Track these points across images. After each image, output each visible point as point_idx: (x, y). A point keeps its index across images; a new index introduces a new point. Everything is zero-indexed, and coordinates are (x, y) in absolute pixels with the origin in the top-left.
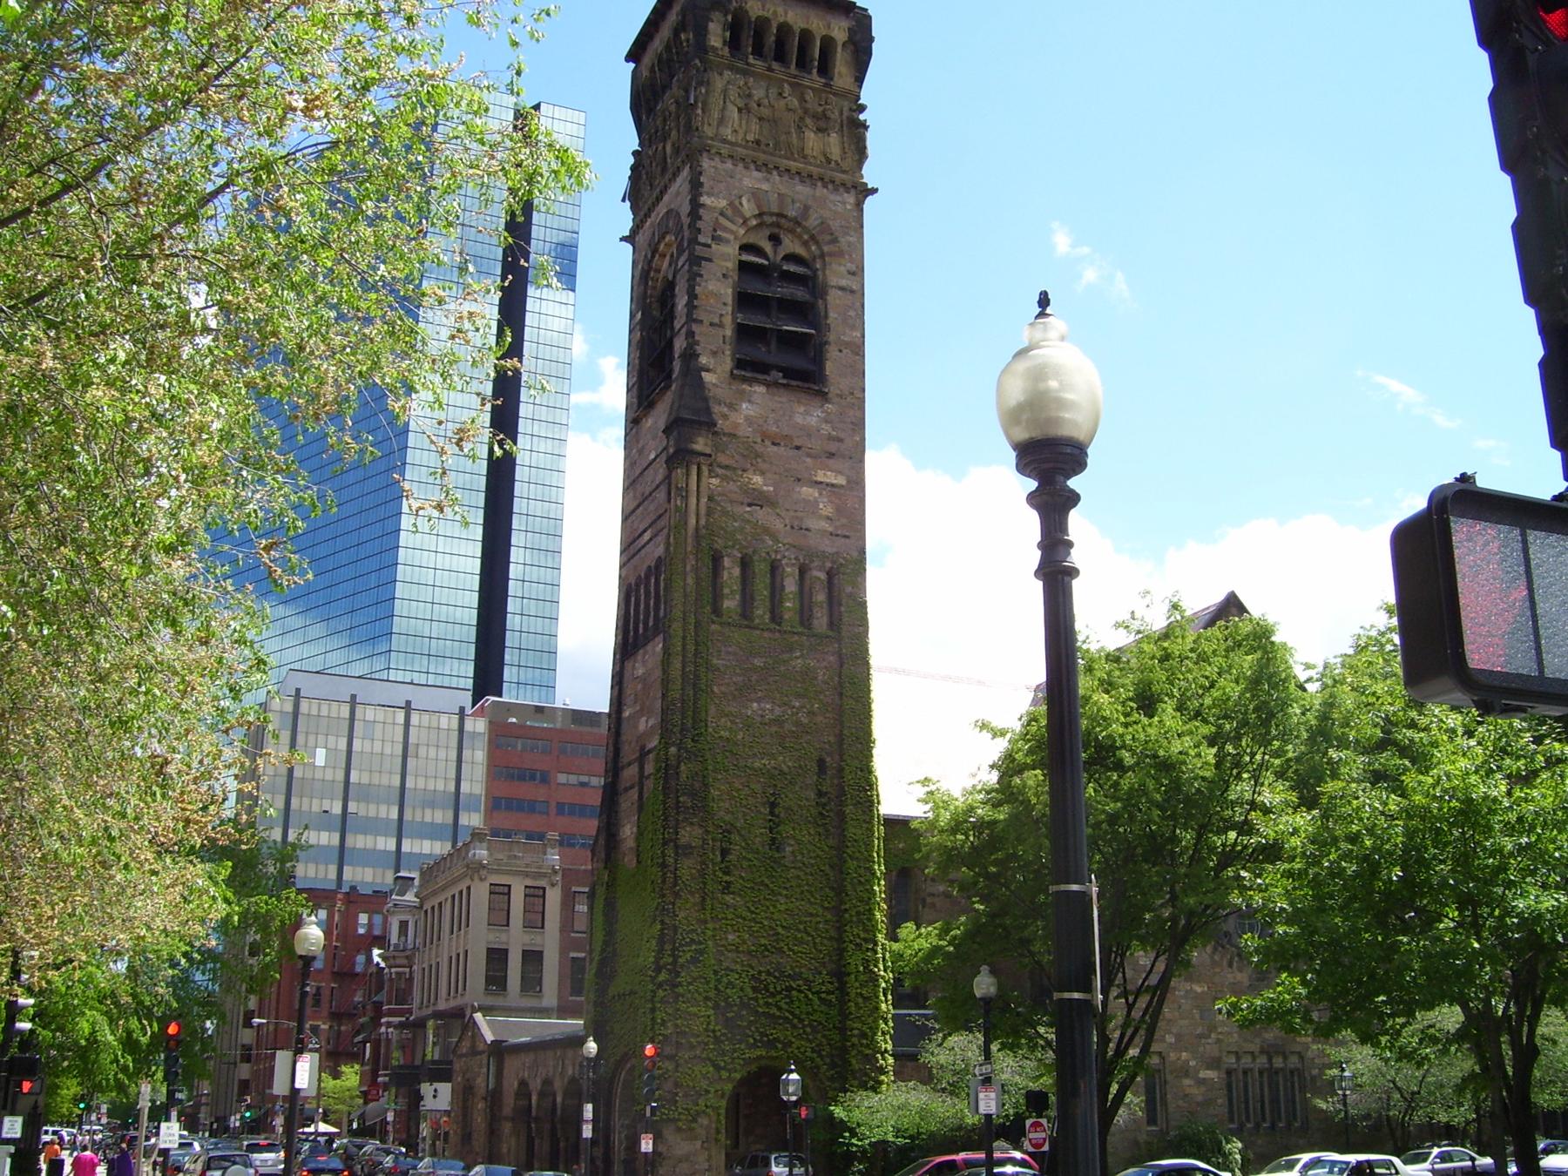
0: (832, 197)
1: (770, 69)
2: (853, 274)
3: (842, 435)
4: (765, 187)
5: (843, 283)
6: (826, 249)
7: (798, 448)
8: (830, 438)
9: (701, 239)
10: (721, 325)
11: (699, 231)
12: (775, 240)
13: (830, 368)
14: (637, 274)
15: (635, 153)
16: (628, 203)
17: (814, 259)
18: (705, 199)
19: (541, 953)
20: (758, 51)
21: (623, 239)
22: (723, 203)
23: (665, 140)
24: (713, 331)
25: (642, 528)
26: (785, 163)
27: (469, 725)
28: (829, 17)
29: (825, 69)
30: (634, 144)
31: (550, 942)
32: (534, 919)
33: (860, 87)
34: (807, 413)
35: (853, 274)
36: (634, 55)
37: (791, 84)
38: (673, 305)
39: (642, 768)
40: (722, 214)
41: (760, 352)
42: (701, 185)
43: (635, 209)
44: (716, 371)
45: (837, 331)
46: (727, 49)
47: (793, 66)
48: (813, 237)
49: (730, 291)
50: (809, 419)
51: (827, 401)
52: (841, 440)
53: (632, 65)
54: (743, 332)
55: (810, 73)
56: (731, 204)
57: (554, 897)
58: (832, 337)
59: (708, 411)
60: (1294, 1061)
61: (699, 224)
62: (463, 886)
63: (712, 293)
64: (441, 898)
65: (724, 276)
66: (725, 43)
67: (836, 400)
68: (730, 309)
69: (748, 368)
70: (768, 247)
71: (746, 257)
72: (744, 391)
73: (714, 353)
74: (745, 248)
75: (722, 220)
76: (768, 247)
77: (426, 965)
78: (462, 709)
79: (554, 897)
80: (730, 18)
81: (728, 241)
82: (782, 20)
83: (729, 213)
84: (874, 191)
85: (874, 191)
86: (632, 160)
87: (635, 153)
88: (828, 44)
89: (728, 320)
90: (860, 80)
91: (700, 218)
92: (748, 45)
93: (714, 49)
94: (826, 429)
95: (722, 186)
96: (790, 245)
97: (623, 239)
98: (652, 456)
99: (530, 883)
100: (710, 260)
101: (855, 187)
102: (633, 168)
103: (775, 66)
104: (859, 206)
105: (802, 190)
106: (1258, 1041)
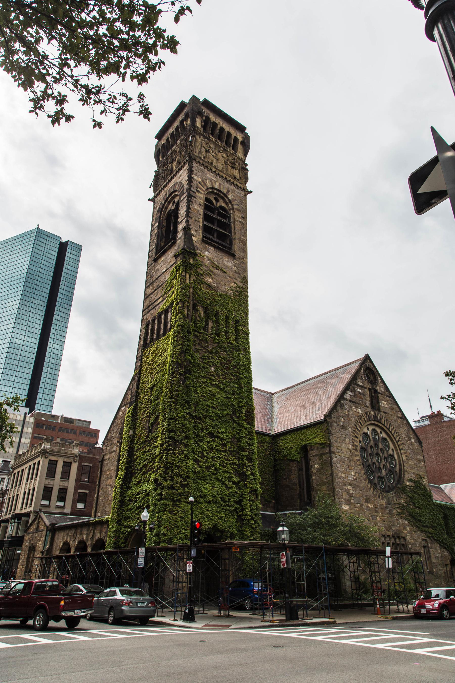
1: (216, 141)
2: (244, 218)
3: (240, 272)
6: (235, 207)
8: (236, 272)
9: (192, 189)
11: (192, 186)
12: (217, 200)
14: (156, 211)
15: (156, 172)
17: (230, 210)
18: (193, 176)
19: (66, 489)
21: (150, 200)
22: (200, 180)
23: (172, 163)
25: (156, 298)
27: (27, 419)
28: (236, 131)
29: (235, 148)
30: (156, 168)
31: (71, 484)
32: (66, 475)
33: (246, 158)
34: (228, 261)
35: (244, 218)
36: (159, 137)
37: (223, 148)
40: (200, 183)
42: (193, 171)
43: (155, 190)
45: (236, 236)
46: (202, 128)
48: (230, 202)
49: (202, 210)
52: (240, 274)
53: (157, 141)
55: (229, 147)
56: (203, 181)
57: (74, 467)
60: (402, 541)
61: (192, 184)
62: (36, 461)
64: (24, 467)
66: (202, 126)
67: (238, 260)
69: (206, 241)
72: (206, 247)
73: (196, 231)
75: (199, 185)
77: (11, 496)
78: (26, 414)
79: (74, 467)
80: (204, 118)
82: (221, 126)
83: (202, 183)
84: (251, 192)
85: (251, 192)
86: (155, 174)
87: (156, 172)
88: (236, 139)
90: (245, 155)
91: (192, 182)
92: (209, 129)
96: (221, 203)
97: (150, 200)
98: (164, 270)
99: (66, 460)
100: (195, 197)
101: (244, 189)
102: (155, 176)
104: (246, 195)
105: (227, 185)
106: (391, 530)
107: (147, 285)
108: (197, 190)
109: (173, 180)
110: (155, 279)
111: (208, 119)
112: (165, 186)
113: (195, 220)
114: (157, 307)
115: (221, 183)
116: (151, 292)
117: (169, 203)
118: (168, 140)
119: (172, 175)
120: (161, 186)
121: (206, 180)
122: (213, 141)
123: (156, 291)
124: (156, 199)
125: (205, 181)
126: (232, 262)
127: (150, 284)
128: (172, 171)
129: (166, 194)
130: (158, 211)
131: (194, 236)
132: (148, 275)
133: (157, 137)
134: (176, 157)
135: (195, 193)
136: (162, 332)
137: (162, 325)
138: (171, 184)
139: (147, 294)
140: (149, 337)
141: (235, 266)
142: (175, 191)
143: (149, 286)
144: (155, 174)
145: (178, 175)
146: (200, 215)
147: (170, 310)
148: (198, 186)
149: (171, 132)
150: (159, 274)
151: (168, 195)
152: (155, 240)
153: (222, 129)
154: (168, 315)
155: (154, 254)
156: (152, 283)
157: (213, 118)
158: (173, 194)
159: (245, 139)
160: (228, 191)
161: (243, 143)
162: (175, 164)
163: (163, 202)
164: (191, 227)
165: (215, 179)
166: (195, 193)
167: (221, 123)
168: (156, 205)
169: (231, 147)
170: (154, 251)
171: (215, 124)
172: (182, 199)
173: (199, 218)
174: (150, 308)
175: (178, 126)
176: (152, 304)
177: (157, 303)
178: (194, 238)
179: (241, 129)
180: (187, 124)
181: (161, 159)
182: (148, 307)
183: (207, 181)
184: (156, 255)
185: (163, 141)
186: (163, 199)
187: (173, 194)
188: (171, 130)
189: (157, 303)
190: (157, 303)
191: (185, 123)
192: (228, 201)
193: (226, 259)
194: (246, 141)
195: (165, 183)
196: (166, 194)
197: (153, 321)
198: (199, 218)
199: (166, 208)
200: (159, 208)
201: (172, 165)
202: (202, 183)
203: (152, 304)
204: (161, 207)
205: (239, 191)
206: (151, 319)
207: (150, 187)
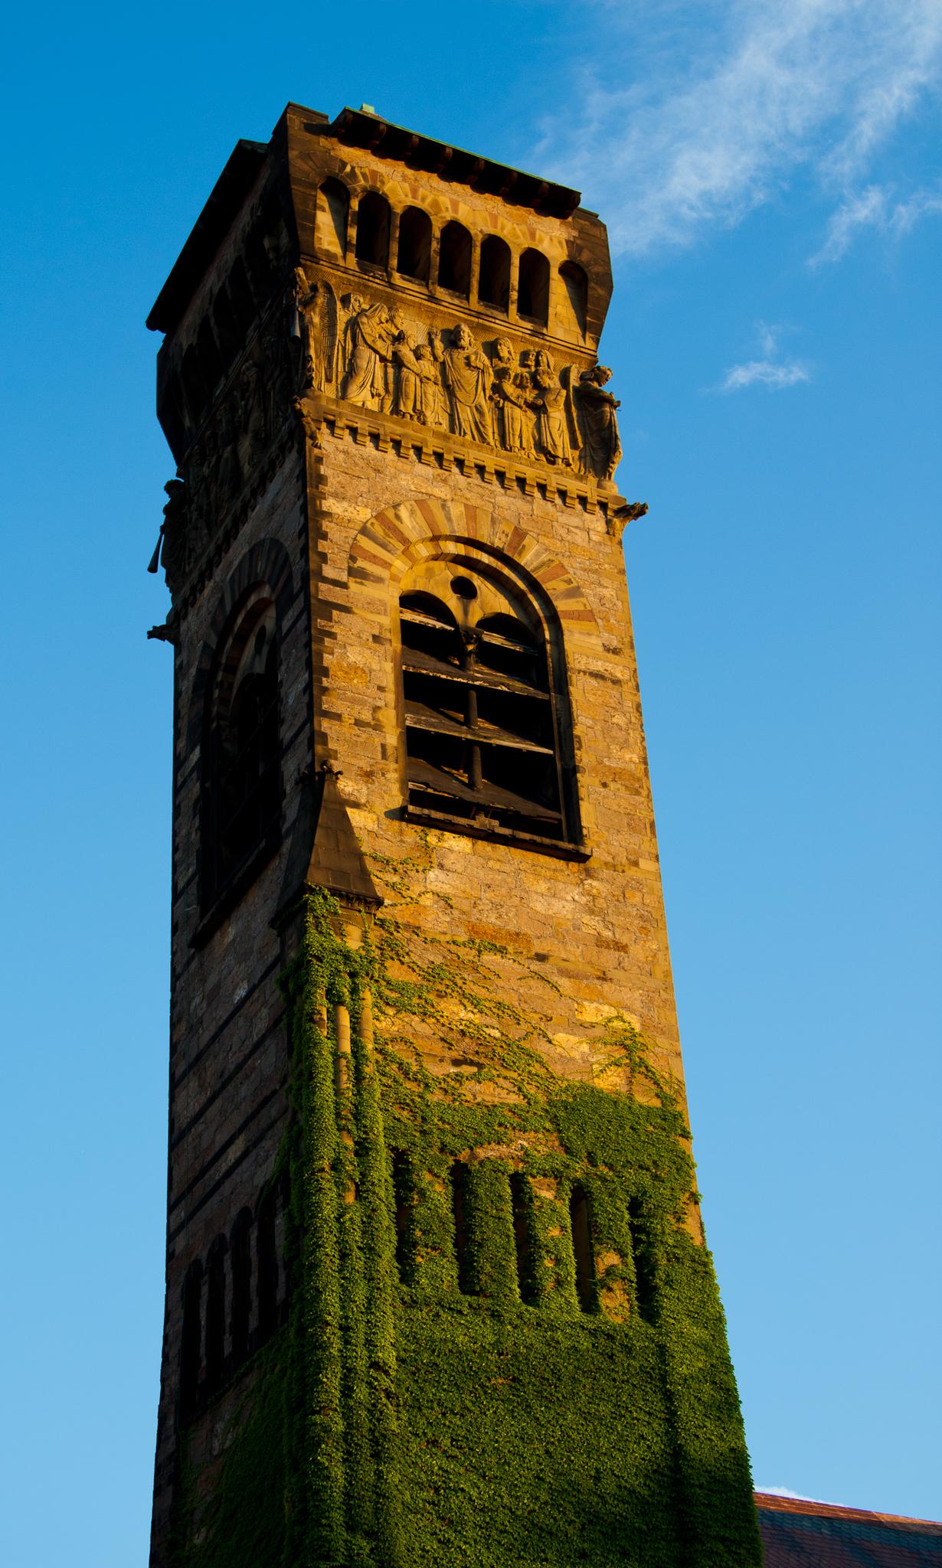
0: (563, 519)
1: (432, 298)
2: (615, 651)
3: (624, 939)
4: (441, 492)
5: (598, 666)
7: (541, 958)
8: (601, 943)
9: (328, 571)
10: (377, 727)
12: (464, 589)
13: (588, 814)
14: (187, 685)
15: (170, 487)
16: (162, 571)
20: (411, 267)
21: (156, 633)
22: (364, 514)
23: (234, 440)
24: (364, 735)
25: (221, 1139)
26: (472, 456)
29: (534, 307)
30: (169, 470)
38: (279, 700)
39: (448, 538)
40: (364, 531)
41: (452, 783)
44: (369, 789)
46: (352, 260)
47: (474, 297)
49: (389, 666)
50: (557, 905)
51: (589, 874)
52: (621, 948)
53: (158, 337)
54: (416, 743)
56: (380, 517)
58: (584, 757)
59: (364, 875)
63: (355, 668)
65: (376, 639)
67: (606, 873)
68: (390, 697)
69: (425, 809)
70: (452, 601)
71: (410, 616)
73: (368, 775)
74: (410, 600)
75: (365, 542)
76: (452, 601)
81: (379, 580)
82: (449, 216)
83: (378, 530)
87: (170, 487)
88: (534, 261)
89: (389, 717)
93: (330, 256)
94: (592, 924)
95: (363, 486)
97: (156, 633)
98: (241, 992)
100: (346, 610)
103: (441, 293)
105: (509, 502)
107: (179, 1072)
108: (352, 572)
109: (246, 529)
110: (206, 1038)
111: (375, 201)
112: (212, 564)
113: (358, 723)
114: (227, 1188)
115: (475, 501)
116: (195, 1107)
117: (241, 640)
118: (204, 328)
119: (239, 504)
120: (197, 560)
121: (396, 506)
122: (412, 304)
123: (218, 1103)
124: (184, 627)
125: (390, 514)
126: (575, 893)
127: (190, 1067)
128: (236, 479)
129: (222, 600)
130: (195, 689)
131: (356, 805)
132: (179, 1021)
133: (154, 322)
134: (248, 414)
135: (344, 586)
136: (253, 1322)
137: (254, 1281)
138: (238, 550)
139: (183, 1122)
140: (202, 1350)
141: (592, 912)
142: (255, 586)
143: (185, 1074)
144: (166, 499)
145: (262, 506)
146: (381, 689)
147: (280, 1201)
148: (354, 546)
149: (216, 290)
150: (223, 1013)
151: (228, 608)
152: (195, 837)
153: (455, 232)
154: (273, 1226)
155: (194, 908)
156: (199, 1057)
157: (402, 185)
158: (253, 599)
159: (580, 249)
160: (519, 534)
161: (572, 271)
162: (245, 446)
163: (213, 642)
164: (336, 766)
165: (441, 492)
166: (344, 586)
167: (445, 201)
168: (184, 655)
169: (513, 308)
170: (193, 889)
171: (416, 218)
172: (286, 625)
173: (376, 709)
174: (199, 1191)
175: (239, 258)
176: (204, 1171)
177: (223, 1166)
178: (356, 817)
179: (557, 202)
180: (276, 248)
181: (187, 423)
182: (191, 1187)
183: (404, 512)
184: (202, 918)
185: (186, 338)
186: (213, 624)
187: (253, 599)
188: (213, 281)
189: (224, 1168)
190: (223, 1166)
191: (266, 243)
192: (521, 585)
193: (543, 886)
194: (585, 256)
195: (212, 547)
196: (222, 600)
197: (216, 1258)
198: (376, 709)
199: (232, 669)
200: (199, 671)
201: (235, 453)
202: (378, 530)
203: (204, 1171)
204: (207, 666)
205: (575, 521)
206: (204, 1255)
207: (153, 569)
